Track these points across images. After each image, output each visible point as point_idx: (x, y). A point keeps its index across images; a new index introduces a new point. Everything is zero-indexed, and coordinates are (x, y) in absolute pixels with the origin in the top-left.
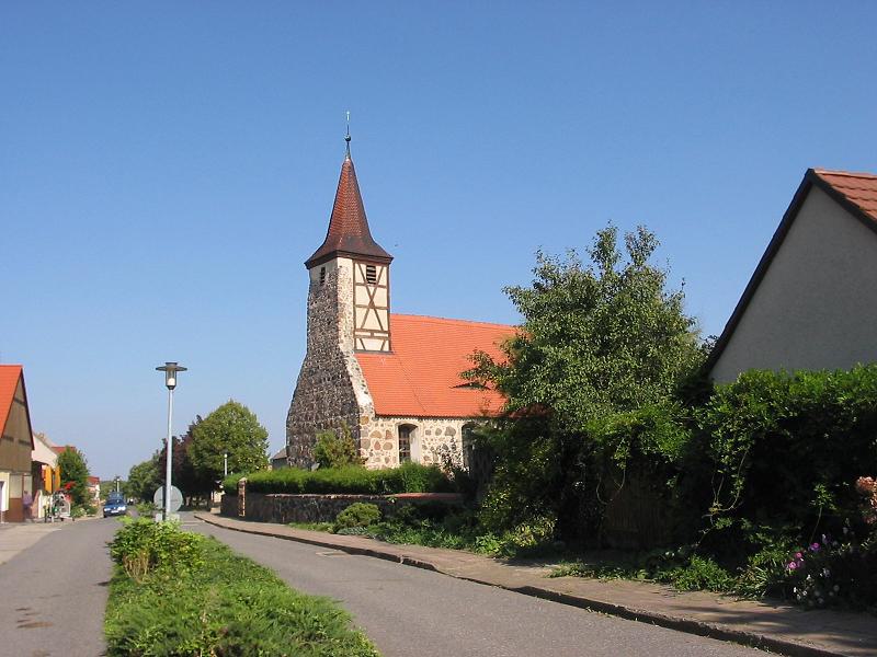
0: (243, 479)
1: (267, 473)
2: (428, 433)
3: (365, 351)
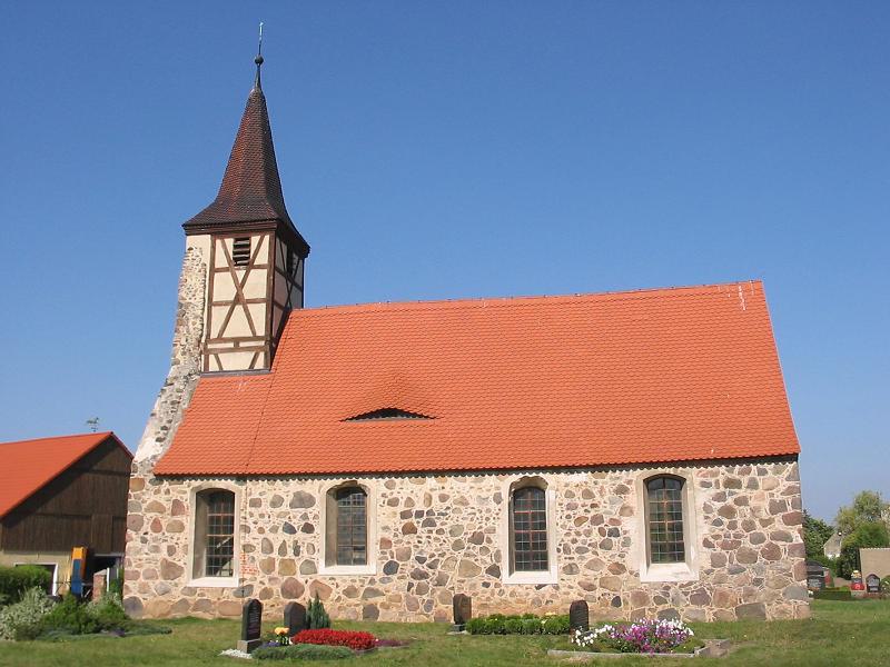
2: (255, 503)
3: (221, 372)
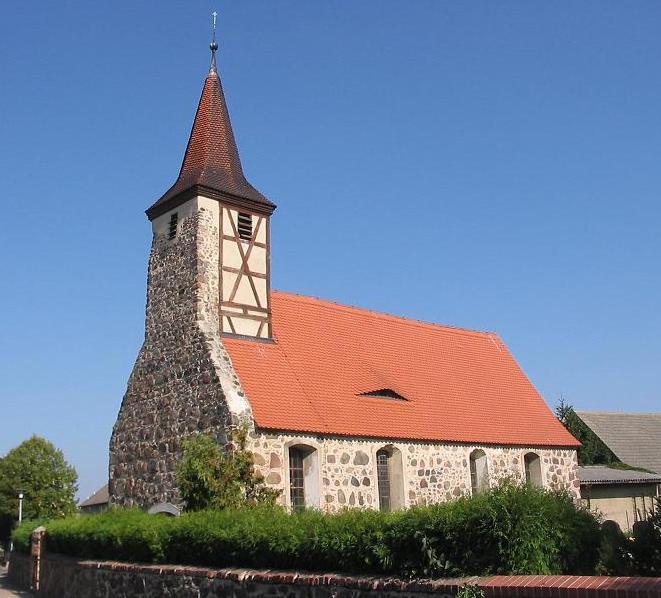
0: (41, 529)
1: (73, 523)
2: (331, 459)
3: (234, 335)
